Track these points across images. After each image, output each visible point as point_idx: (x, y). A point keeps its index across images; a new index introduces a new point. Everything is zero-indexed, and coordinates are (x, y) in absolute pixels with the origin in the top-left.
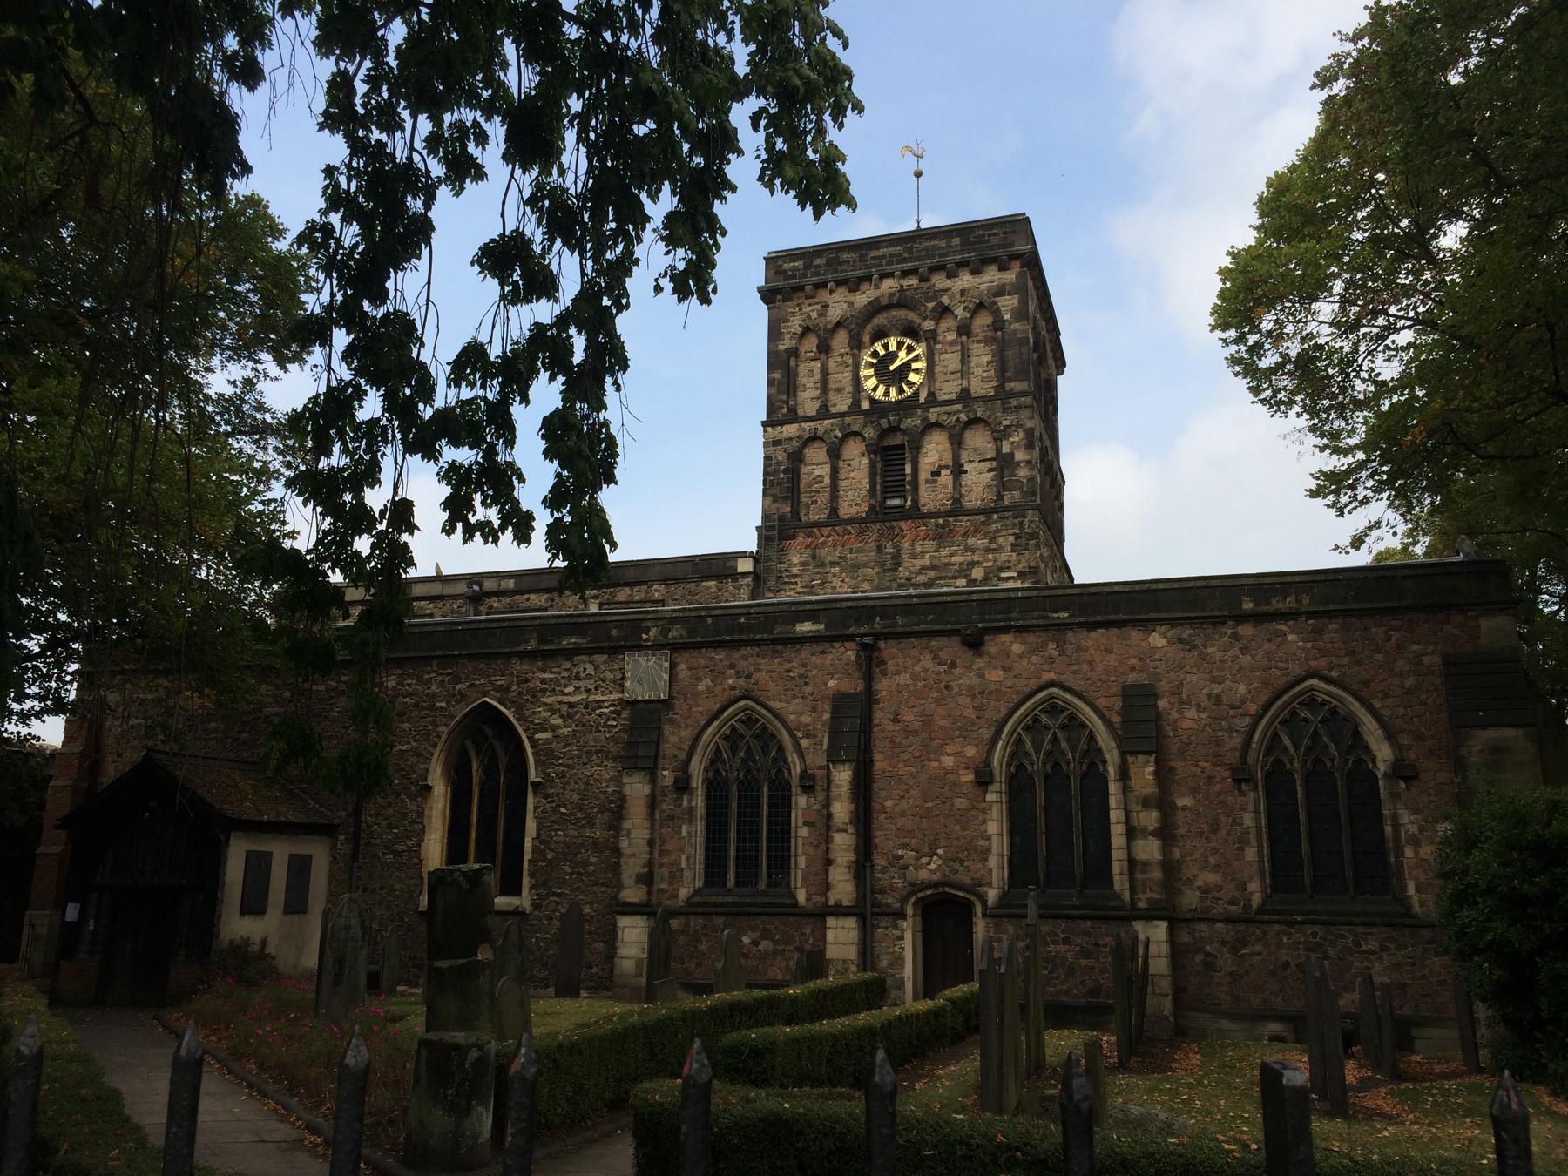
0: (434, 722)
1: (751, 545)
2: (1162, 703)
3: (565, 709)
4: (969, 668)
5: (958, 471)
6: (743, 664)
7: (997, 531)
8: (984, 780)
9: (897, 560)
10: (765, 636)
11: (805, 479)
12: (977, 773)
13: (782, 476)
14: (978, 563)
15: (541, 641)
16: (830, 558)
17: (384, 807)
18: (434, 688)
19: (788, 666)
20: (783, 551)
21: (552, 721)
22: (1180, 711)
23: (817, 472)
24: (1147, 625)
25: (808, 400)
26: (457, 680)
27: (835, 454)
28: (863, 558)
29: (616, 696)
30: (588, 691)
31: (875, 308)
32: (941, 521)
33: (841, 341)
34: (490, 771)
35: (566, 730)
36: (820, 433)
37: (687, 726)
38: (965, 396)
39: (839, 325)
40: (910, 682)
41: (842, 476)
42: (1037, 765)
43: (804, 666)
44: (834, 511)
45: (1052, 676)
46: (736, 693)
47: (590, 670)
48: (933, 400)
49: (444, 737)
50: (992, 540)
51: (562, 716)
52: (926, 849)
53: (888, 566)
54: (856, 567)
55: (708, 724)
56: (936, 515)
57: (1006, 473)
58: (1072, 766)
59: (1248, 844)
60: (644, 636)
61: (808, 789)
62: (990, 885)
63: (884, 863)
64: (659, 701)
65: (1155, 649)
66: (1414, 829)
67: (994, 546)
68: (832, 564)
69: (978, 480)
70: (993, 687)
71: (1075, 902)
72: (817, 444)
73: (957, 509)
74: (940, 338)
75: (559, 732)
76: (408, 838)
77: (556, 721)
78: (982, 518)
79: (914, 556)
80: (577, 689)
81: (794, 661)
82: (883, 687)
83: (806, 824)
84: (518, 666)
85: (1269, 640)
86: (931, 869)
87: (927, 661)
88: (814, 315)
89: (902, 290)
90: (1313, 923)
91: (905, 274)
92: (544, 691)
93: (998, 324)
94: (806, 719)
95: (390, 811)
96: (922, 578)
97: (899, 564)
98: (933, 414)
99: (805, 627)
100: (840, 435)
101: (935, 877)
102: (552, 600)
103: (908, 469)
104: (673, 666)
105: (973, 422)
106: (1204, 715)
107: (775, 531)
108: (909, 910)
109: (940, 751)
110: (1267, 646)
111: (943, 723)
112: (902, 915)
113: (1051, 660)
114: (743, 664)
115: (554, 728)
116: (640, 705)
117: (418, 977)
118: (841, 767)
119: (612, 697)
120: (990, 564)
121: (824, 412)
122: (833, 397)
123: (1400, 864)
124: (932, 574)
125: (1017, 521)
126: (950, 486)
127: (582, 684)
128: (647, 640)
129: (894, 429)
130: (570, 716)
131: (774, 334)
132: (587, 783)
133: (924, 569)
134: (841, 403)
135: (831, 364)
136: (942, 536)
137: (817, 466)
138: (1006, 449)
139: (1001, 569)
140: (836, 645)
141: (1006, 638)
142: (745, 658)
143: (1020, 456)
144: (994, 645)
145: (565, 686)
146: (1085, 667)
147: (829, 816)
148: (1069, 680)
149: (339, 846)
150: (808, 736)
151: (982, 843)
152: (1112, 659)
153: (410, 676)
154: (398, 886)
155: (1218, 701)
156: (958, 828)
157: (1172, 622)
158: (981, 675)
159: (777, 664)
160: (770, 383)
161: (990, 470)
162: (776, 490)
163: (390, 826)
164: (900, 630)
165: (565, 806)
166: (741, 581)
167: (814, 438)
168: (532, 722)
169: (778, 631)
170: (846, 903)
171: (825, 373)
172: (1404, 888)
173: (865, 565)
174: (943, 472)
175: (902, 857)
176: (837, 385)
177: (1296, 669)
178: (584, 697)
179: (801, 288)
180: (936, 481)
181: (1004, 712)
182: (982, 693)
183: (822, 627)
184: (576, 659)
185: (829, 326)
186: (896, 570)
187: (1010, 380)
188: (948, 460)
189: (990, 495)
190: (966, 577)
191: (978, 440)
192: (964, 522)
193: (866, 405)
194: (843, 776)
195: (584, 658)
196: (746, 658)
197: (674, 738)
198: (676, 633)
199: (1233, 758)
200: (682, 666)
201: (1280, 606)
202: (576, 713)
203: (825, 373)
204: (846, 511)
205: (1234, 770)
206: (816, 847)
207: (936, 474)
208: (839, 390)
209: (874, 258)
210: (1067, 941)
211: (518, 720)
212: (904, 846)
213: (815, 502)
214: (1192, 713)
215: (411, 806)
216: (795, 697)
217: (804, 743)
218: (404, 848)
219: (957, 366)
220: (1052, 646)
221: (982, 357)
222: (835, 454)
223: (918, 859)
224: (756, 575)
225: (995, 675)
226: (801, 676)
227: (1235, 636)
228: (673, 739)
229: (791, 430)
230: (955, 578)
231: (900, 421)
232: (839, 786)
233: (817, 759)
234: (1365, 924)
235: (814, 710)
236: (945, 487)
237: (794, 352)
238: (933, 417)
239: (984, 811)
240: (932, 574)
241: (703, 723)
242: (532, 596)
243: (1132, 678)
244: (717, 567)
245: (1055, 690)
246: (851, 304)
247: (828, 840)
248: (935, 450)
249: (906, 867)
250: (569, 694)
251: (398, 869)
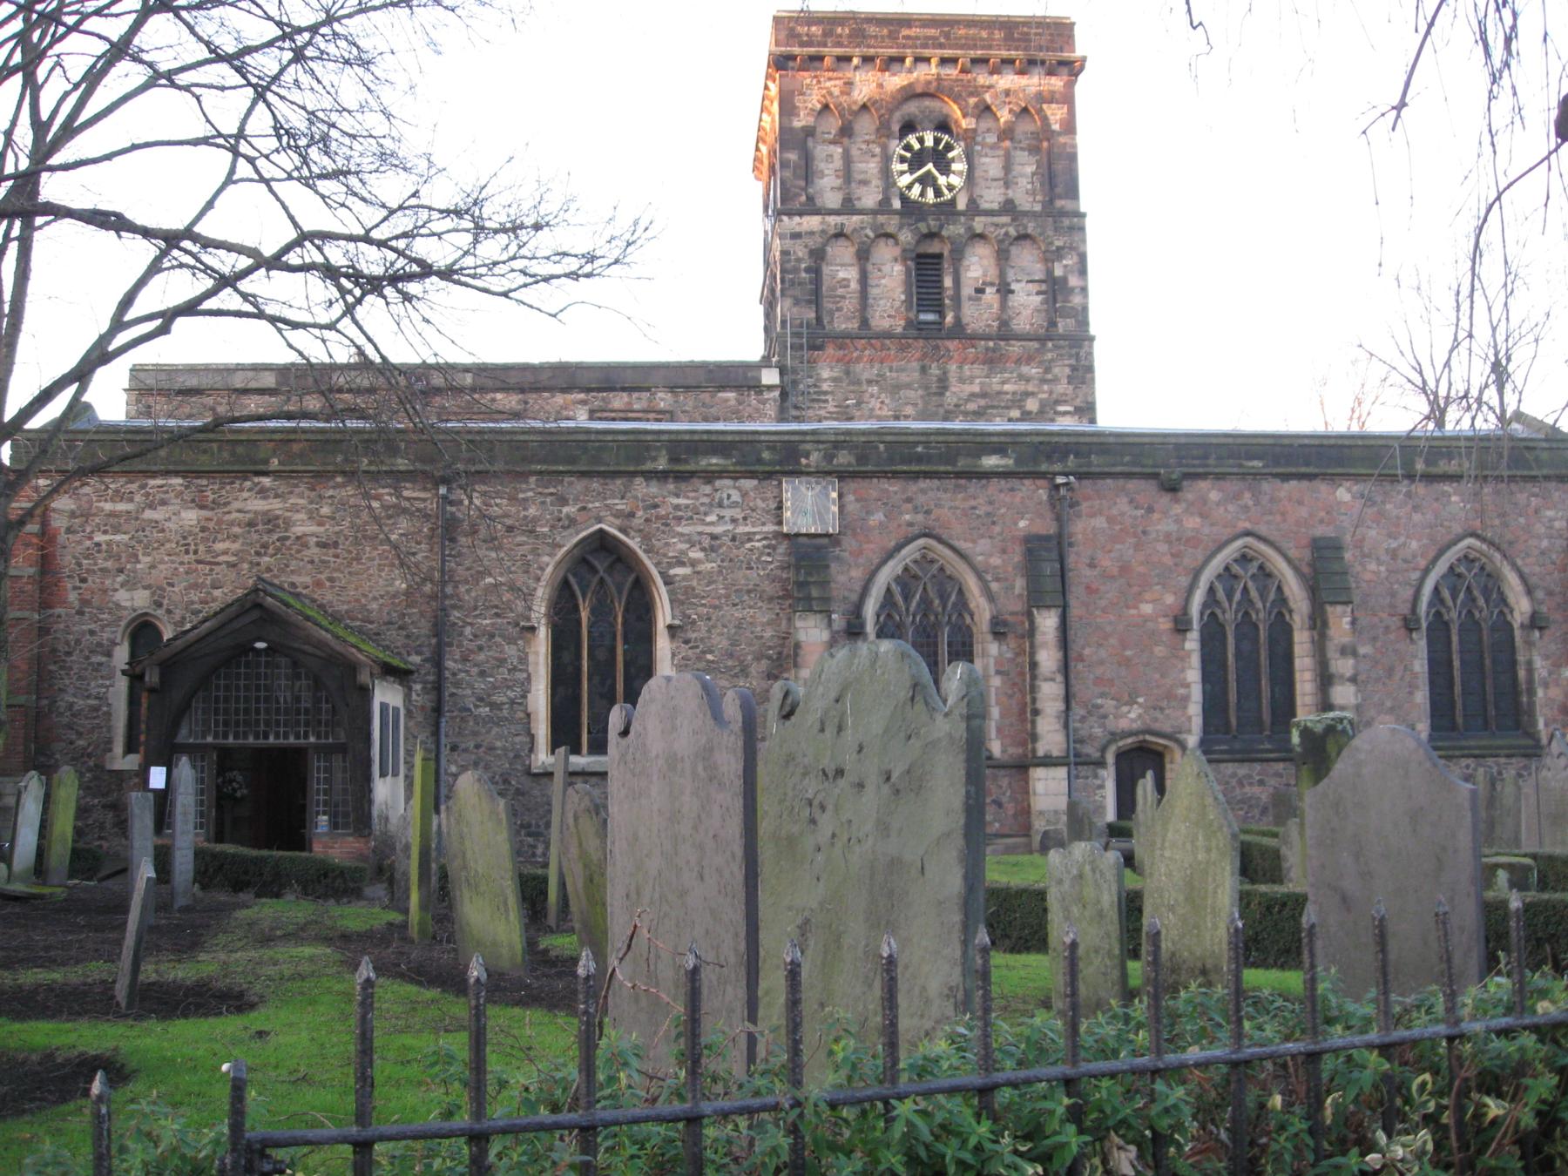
0: (534, 551)
2: (1348, 556)
3: (706, 542)
4: (1165, 513)
5: (1005, 290)
6: (921, 499)
7: (1052, 360)
8: (1181, 626)
10: (949, 468)
11: (826, 283)
12: (1176, 620)
13: (803, 275)
14: (1033, 394)
15: (674, 460)
16: (866, 376)
17: (472, 651)
18: (532, 511)
19: (973, 503)
20: (812, 362)
21: (692, 555)
22: (1363, 565)
23: (841, 275)
24: (1333, 479)
25: (828, 188)
26: (563, 501)
27: (863, 256)
28: (904, 378)
29: (770, 528)
30: (734, 521)
31: (909, 94)
32: (991, 344)
34: (601, 612)
35: (709, 566)
36: (847, 230)
37: (857, 566)
38: (1008, 207)
40: (1105, 525)
41: (872, 282)
42: (1229, 617)
43: (991, 503)
44: (865, 323)
45: (1248, 525)
46: (916, 530)
47: (736, 497)
48: (974, 209)
49: (549, 570)
50: (1048, 370)
51: (703, 549)
52: (1126, 698)
53: (934, 390)
54: (897, 388)
55: (884, 562)
56: (987, 338)
57: (1059, 298)
58: (1261, 615)
59: (1417, 687)
60: (804, 461)
62: (1189, 731)
63: (1082, 712)
64: (827, 535)
65: (1339, 503)
66: (1544, 673)
67: (1049, 376)
68: (869, 382)
70: (1190, 534)
71: (1268, 746)
72: (842, 242)
73: (1005, 333)
74: (979, 139)
75: (700, 568)
76: (508, 687)
77: (696, 554)
78: (1035, 345)
79: (962, 380)
80: (721, 518)
81: (981, 496)
82: (1079, 528)
83: (998, 672)
84: (641, 487)
85: (1437, 499)
86: (1131, 717)
87: (1122, 505)
88: (836, 92)
89: (939, 79)
90: (1467, 756)
91: (944, 61)
92: (680, 519)
94: (996, 561)
95: (481, 657)
96: (972, 406)
97: (946, 388)
98: (979, 224)
99: (991, 462)
100: (871, 235)
101: (1135, 726)
102: (526, 403)
103: (948, 282)
105: (1023, 237)
106: (1383, 569)
108: (1110, 758)
109: (1139, 598)
110: (1435, 505)
111: (1141, 569)
112: (1101, 763)
113: (1246, 508)
114: (921, 499)
115: (693, 563)
116: (801, 540)
117: (535, 847)
118: (1045, 613)
119: (765, 529)
120: (1045, 396)
121: (848, 207)
123: (1531, 704)
124: (982, 402)
125: (1074, 351)
126: (996, 306)
127: (727, 513)
128: (808, 465)
129: (932, 235)
130: (713, 549)
132: (738, 627)
133: (973, 395)
134: (869, 198)
135: (855, 152)
136: (993, 361)
137: (842, 270)
138: (1058, 272)
139: (1057, 402)
140: (1027, 482)
141: (1203, 485)
142: (924, 491)
144: (1191, 491)
145: (706, 514)
146: (1278, 518)
147: (1034, 665)
148: (1263, 530)
149: (414, 697)
150: (997, 580)
151: (1181, 691)
152: (1303, 512)
153: (499, 495)
154: (498, 744)
155: (1394, 554)
156: (1157, 676)
157: (1356, 477)
158: (1178, 521)
159: (959, 500)
161: (1038, 293)
162: (797, 292)
163: (482, 674)
164: (1098, 470)
165: (711, 652)
166: (766, 395)
167: (840, 235)
168: (665, 555)
169: (962, 463)
170: (1056, 753)
171: (847, 159)
172: (1534, 723)
173: (908, 386)
174: (988, 290)
175: (1101, 706)
176: (862, 177)
177: (1458, 529)
178: (730, 527)
179: (821, 58)
180: (979, 299)
181: (1201, 558)
182: (1179, 539)
183: (1011, 462)
184: (718, 483)
185: (855, 108)
186: (942, 394)
187: (1060, 197)
188: (993, 274)
189: (1040, 320)
190: (1020, 407)
192: (1015, 348)
194: (1048, 622)
195: (728, 482)
196: (927, 492)
197: (844, 577)
198: (844, 459)
199: (1405, 609)
200: (850, 498)
201: (1447, 468)
202: (720, 546)
205: (1405, 619)
206: (1011, 697)
207: (980, 291)
208: (865, 183)
209: (907, 37)
210: (1261, 783)
211: (645, 551)
212: (1102, 695)
213: (839, 309)
214: (1373, 566)
215: (511, 651)
216: (982, 536)
217: (994, 586)
218: (505, 699)
219: (1000, 174)
220: (1247, 495)
222: (863, 256)
223: (1117, 708)
225: (1192, 522)
226: (988, 514)
227: (1409, 495)
228: (842, 578)
229: (812, 222)
230: (1008, 408)
231: (941, 227)
232: (1044, 633)
234: (1508, 756)
235: (1004, 551)
236: (991, 306)
237: (809, 132)
238: (979, 228)
239: (1182, 659)
240: (982, 402)
241: (876, 561)
242: (499, 396)
243: (1320, 531)
245: (1249, 540)
246: (880, 86)
247: (1033, 689)
248: (977, 266)
249: (1105, 717)
250: (712, 523)
251: (498, 725)
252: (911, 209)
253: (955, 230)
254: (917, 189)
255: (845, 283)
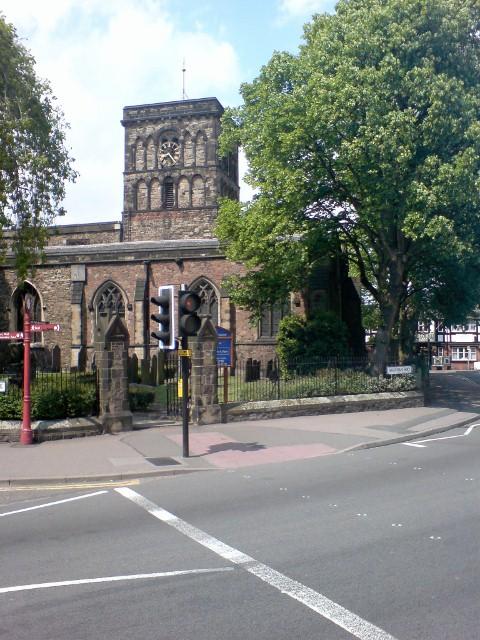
1: (119, 218)
5: (191, 193)
9: (170, 225)
15: (44, 261)
31: (163, 131)
33: (151, 145)
38: (194, 166)
39: (150, 136)
54: (156, 227)
61: (130, 309)
69: (198, 195)
73: (191, 207)
77: (49, 287)
87: (166, 269)
93: (206, 139)
94: (129, 287)
96: (178, 232)
98: (183, 172)
103: (174, 192)
104: (86, 270)
105: (197, 176)
107: (129, 214)
121: (145, 169)
122: (148, 164)
129: (169, 177)
131: (127, 139)
136: (185, 217)
137: (143, 190)
143: (212, 188)
160: (126, 157)
167: (142, 180)
171: (146, 155)
188: (188, 189)
191: (199, 182)
192: (192, 212)
193: (160, 167)
194: (140, 305)
196: (110, 268)
203: (146, 155)
204: (153, 207)
217: (128, 294)
221: (200, 153)
224: (122, 230)
229: (133, 176)
233: (132, 299)
237: (134, 146)
244: (106, 228)
248: (184, 185)
252: (164, 169)
253: (176, 174)
254: (165, 162)
255: (144, 194)
